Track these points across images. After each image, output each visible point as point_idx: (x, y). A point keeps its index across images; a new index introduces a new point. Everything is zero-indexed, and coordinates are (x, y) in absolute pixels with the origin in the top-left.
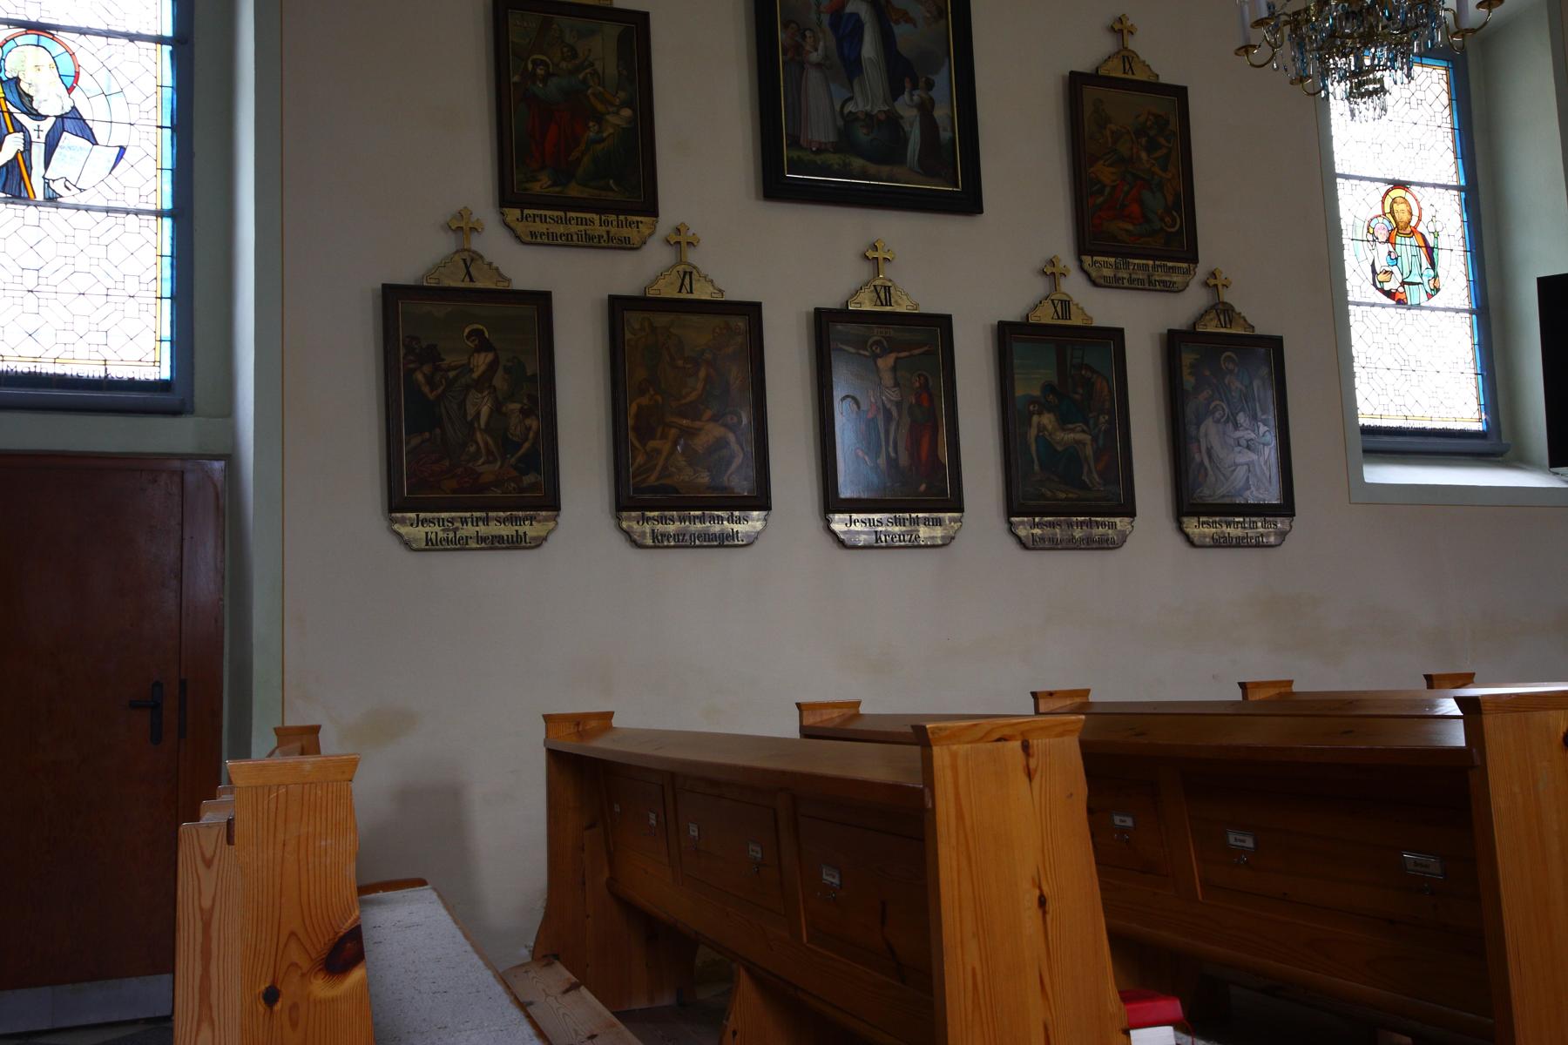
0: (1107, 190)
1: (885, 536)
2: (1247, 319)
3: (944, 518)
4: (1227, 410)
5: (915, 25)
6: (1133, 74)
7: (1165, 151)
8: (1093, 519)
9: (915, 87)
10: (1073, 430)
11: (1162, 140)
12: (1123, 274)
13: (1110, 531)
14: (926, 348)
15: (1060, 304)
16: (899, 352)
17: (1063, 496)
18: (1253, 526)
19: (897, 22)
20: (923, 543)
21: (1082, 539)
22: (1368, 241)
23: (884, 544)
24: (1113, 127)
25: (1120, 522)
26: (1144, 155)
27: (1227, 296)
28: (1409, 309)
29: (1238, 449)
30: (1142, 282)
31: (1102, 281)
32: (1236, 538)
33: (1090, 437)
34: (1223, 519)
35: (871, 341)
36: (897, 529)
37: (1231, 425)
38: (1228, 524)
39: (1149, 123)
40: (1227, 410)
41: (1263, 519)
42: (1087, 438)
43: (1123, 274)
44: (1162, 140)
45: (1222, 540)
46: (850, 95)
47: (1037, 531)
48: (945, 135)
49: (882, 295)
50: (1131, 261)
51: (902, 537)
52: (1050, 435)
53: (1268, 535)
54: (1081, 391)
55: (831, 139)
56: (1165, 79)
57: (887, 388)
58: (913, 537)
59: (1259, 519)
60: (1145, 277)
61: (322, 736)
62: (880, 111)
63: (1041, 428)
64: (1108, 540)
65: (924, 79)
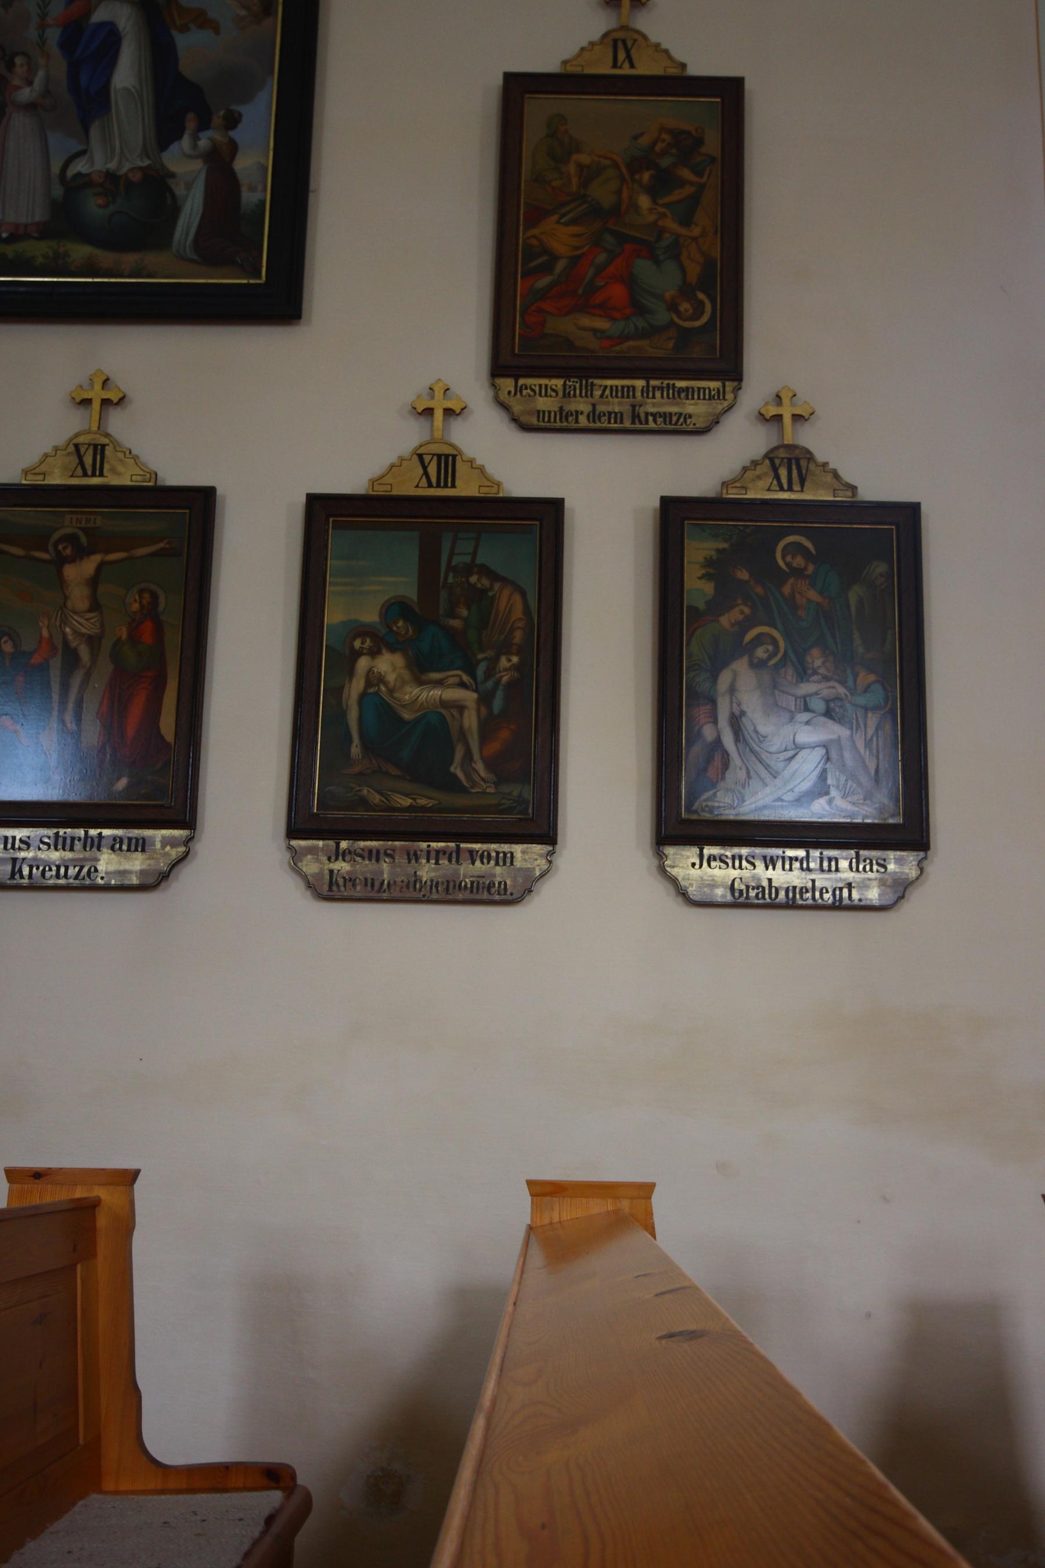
1: (31, 867)
2: (841, 473)
3: (152, 839)
4: (782, 644)
5: (217, 30)
6: (632, 66)
7: (688, 190)
8: (463, 845)
9: (204, 125)
10: (440, 683)
13: (498, 870)
14: (161, 545)
15: (91, 451)
16: (107, 552)
17: (406, 802)
19: (184, 29)
20: (100, 881)
21: (434, 884)
23: (25, 881)
24: (584, 159)
25: (523, 852)
26: (644, 201)
27: (808, 438)
29: (805, 716)
30: (619, 417)
31: (534, 421)
32: (787, 890)
33: (475, 696)
34: (758, 851)
35: (56, 536)
36: (55, 856)
37: (790, 671)
38: (770, 862)
39: (659, 147)
40: (782, 644)
41: (852, 852)
42: (469, 697)
44: (686, 174)
45: (752, 894)
46: (84, 147)
47: (342, 866)
48: (248, 198)
49: (88, 460)
50: (597, 382)
51: (62, 870)
52: (391, 691)
53: (864, 885)
54: (464, 612)
55: (38, 218)
57: (75, 613)
58: (85, 870)
60: (626, 409)
61: (657, 1200)
62: (132, 169)
63: (373, 679)
64: (491, 885)
65: (222, 113)
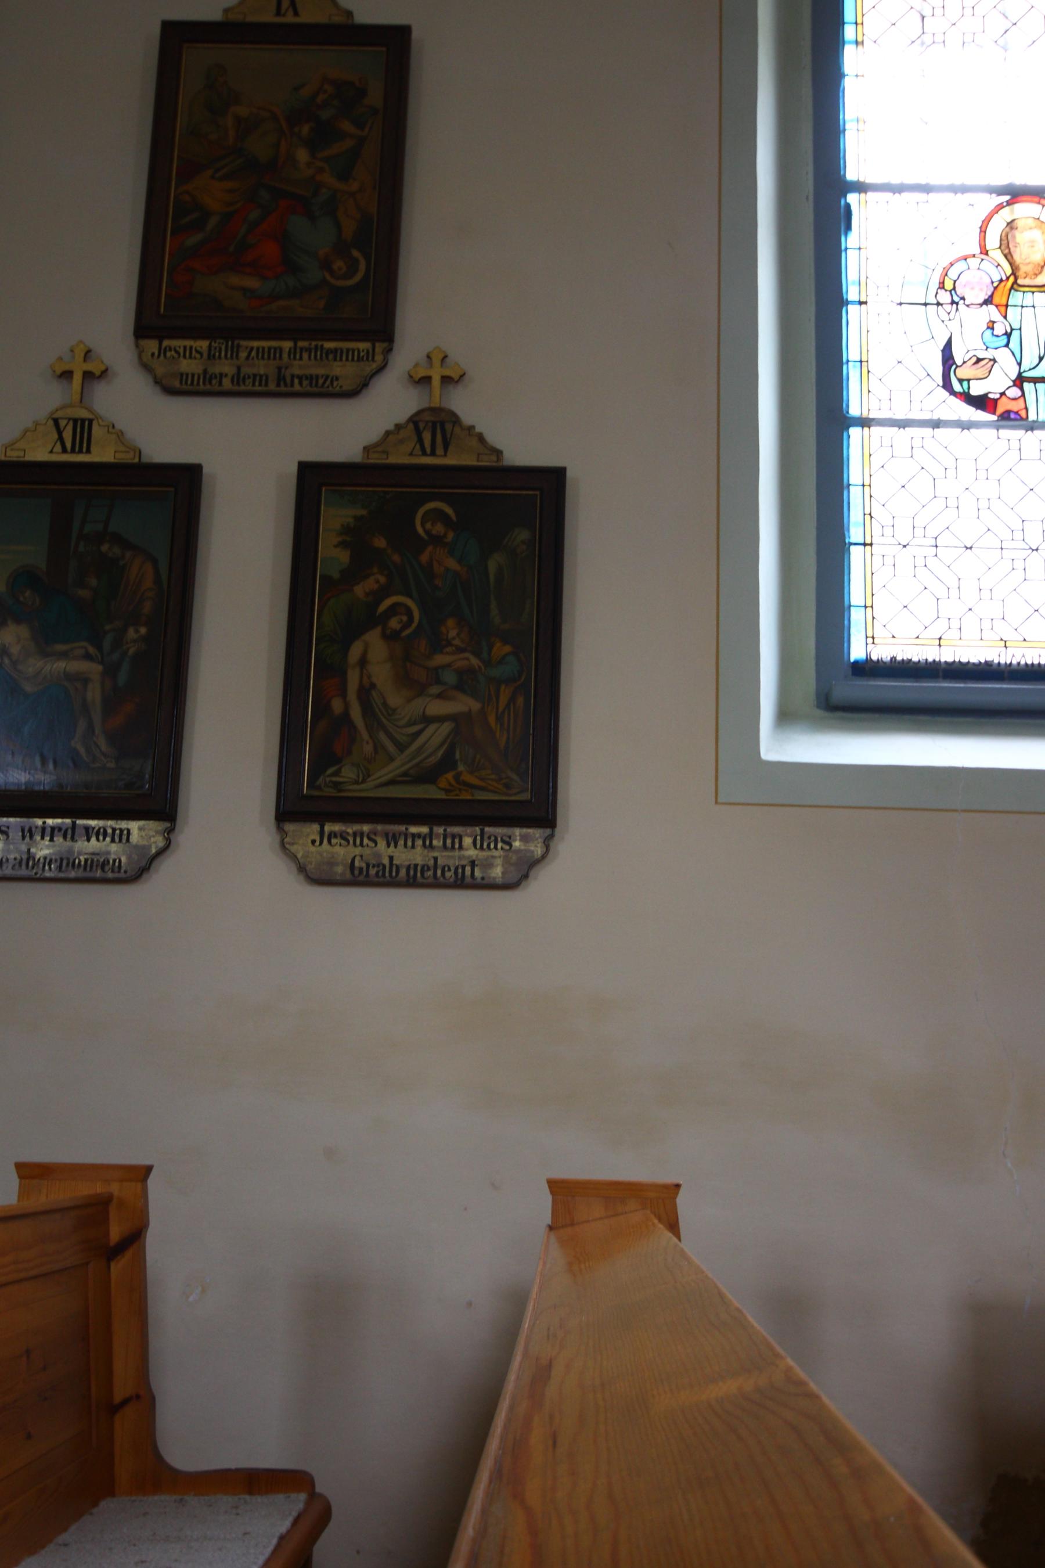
0: (213, 222)
6: (296, 14)
8: (79, 822)
10: (64, 655)
11: (347, 126)
12: (227, 368)
13: (114, 847)
18: (455, 843)
21: (48, 861)
22: (938, 304)
25: (140, 829)
26: (302, 155)
28: (1032, 429)
30: (264, 379)
31: (177, 384)
32: (408, 868)
33: (100, 668)
38: (392, 840)
39: (320, 99)
41: (478, 829)
42: (94, 669)
43: (227, 368)
44: (347, 126)
45: (373, 872)
50: (243, 343)
52: (14, 663)
54: (93, 582)
56: (364, 16)
59: (469, 830)
64: (106, 862)
